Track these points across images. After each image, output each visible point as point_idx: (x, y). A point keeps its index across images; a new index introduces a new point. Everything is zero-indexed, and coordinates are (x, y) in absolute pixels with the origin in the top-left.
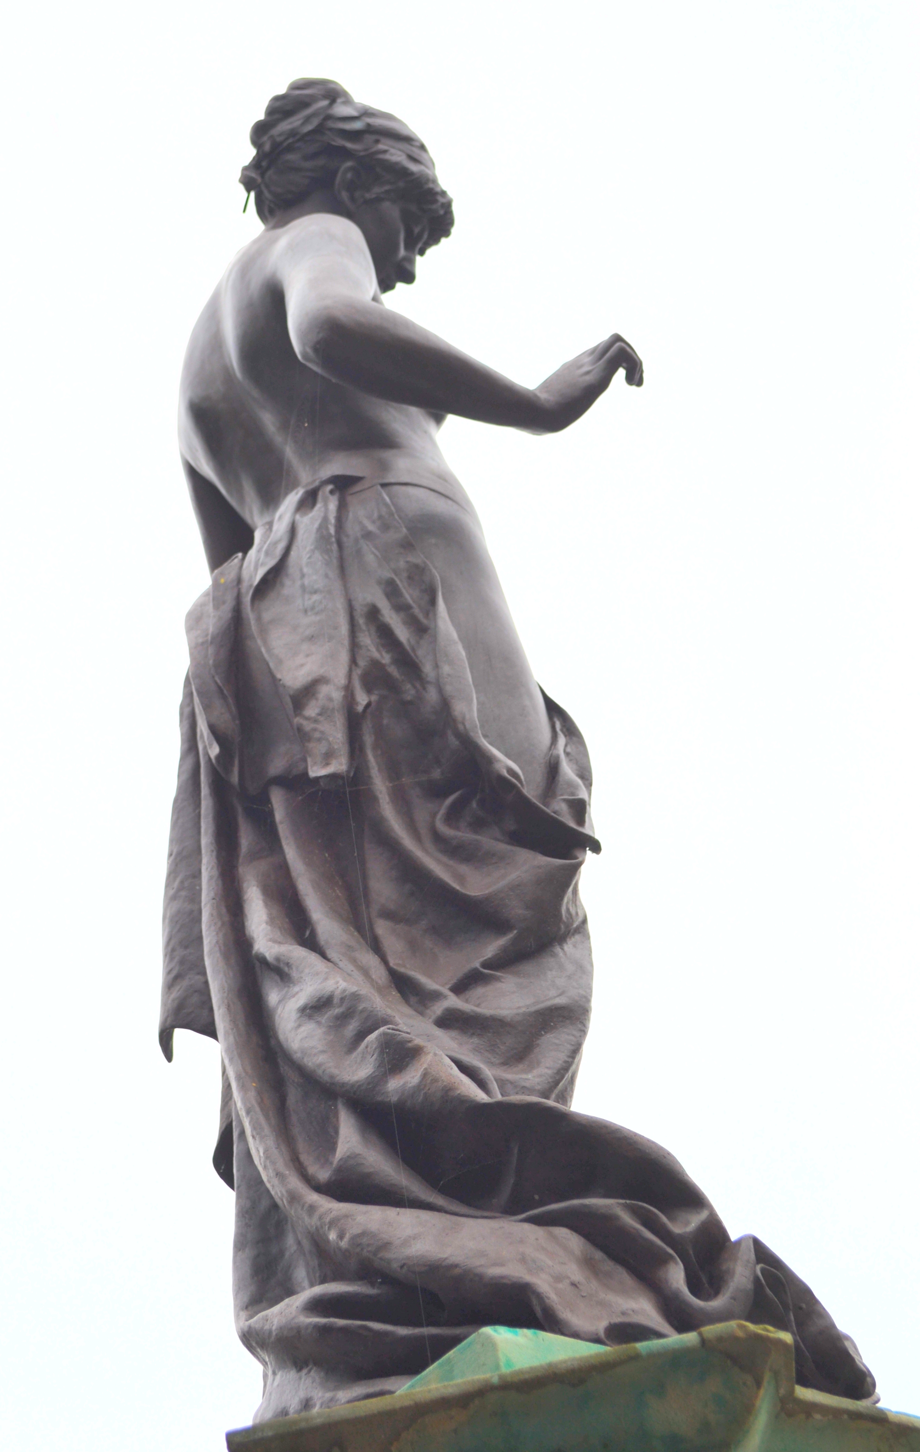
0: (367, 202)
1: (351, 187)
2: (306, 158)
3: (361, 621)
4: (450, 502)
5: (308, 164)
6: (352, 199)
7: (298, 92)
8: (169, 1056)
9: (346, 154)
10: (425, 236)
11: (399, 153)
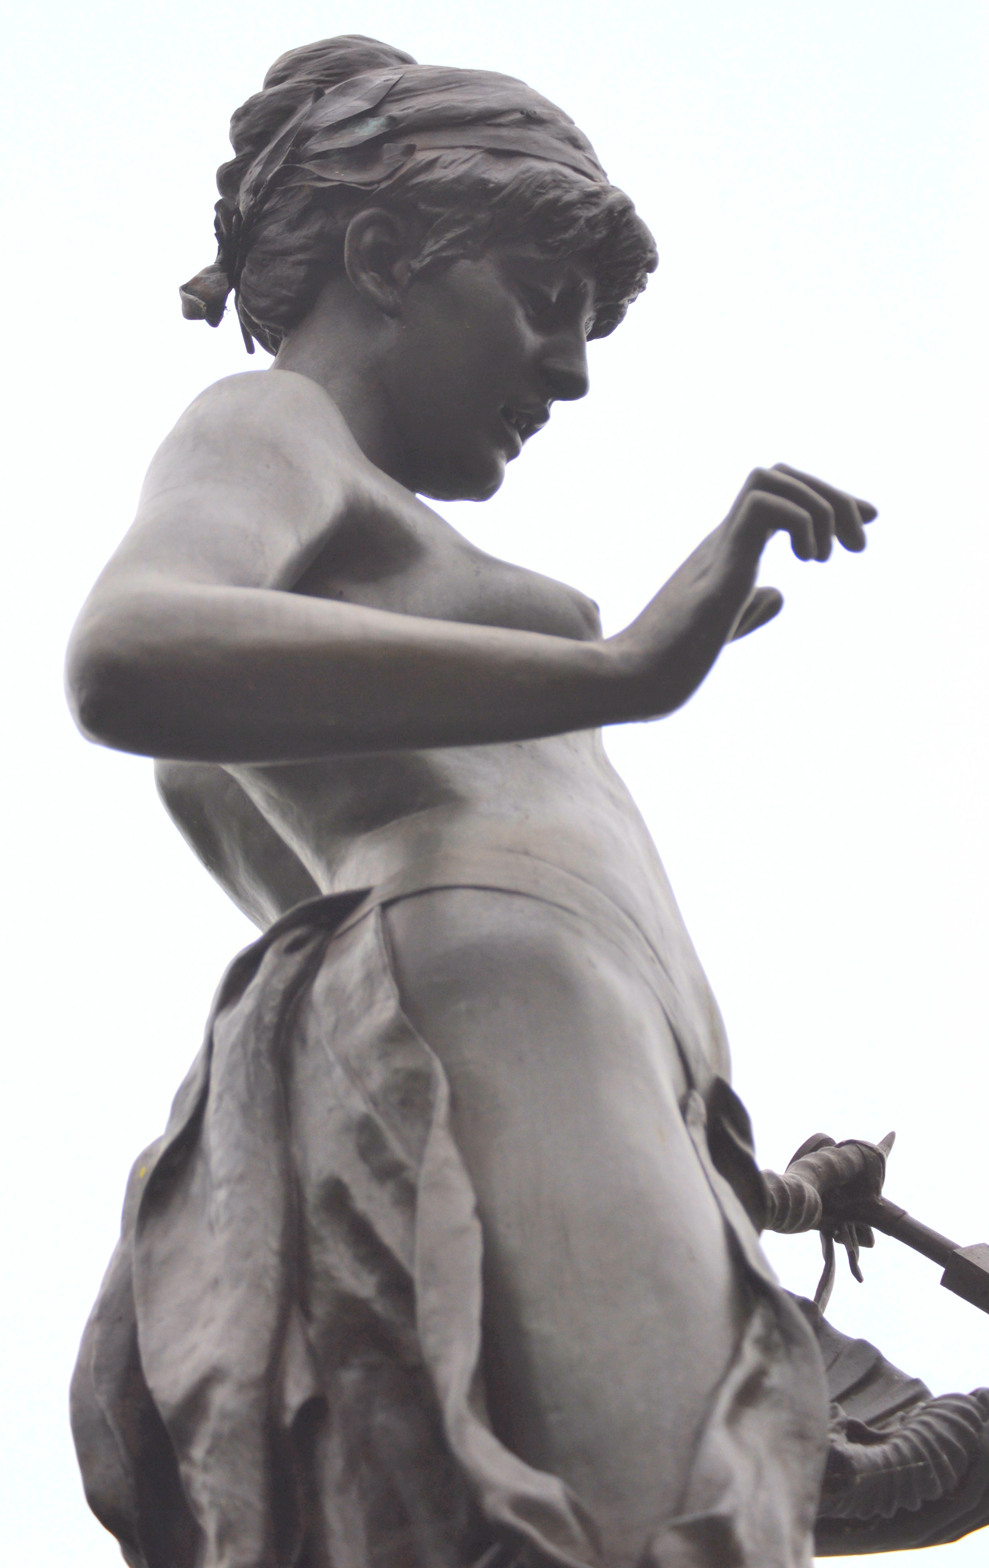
1: (380, 260)
2: (293, 226)
3: (315, 1219)
4: (518, 902)
5: (296, 238)
6: (389, 280)
8: (860, 1279)
9: (348, 197)
10: (590, 285)
11: (464, 154)
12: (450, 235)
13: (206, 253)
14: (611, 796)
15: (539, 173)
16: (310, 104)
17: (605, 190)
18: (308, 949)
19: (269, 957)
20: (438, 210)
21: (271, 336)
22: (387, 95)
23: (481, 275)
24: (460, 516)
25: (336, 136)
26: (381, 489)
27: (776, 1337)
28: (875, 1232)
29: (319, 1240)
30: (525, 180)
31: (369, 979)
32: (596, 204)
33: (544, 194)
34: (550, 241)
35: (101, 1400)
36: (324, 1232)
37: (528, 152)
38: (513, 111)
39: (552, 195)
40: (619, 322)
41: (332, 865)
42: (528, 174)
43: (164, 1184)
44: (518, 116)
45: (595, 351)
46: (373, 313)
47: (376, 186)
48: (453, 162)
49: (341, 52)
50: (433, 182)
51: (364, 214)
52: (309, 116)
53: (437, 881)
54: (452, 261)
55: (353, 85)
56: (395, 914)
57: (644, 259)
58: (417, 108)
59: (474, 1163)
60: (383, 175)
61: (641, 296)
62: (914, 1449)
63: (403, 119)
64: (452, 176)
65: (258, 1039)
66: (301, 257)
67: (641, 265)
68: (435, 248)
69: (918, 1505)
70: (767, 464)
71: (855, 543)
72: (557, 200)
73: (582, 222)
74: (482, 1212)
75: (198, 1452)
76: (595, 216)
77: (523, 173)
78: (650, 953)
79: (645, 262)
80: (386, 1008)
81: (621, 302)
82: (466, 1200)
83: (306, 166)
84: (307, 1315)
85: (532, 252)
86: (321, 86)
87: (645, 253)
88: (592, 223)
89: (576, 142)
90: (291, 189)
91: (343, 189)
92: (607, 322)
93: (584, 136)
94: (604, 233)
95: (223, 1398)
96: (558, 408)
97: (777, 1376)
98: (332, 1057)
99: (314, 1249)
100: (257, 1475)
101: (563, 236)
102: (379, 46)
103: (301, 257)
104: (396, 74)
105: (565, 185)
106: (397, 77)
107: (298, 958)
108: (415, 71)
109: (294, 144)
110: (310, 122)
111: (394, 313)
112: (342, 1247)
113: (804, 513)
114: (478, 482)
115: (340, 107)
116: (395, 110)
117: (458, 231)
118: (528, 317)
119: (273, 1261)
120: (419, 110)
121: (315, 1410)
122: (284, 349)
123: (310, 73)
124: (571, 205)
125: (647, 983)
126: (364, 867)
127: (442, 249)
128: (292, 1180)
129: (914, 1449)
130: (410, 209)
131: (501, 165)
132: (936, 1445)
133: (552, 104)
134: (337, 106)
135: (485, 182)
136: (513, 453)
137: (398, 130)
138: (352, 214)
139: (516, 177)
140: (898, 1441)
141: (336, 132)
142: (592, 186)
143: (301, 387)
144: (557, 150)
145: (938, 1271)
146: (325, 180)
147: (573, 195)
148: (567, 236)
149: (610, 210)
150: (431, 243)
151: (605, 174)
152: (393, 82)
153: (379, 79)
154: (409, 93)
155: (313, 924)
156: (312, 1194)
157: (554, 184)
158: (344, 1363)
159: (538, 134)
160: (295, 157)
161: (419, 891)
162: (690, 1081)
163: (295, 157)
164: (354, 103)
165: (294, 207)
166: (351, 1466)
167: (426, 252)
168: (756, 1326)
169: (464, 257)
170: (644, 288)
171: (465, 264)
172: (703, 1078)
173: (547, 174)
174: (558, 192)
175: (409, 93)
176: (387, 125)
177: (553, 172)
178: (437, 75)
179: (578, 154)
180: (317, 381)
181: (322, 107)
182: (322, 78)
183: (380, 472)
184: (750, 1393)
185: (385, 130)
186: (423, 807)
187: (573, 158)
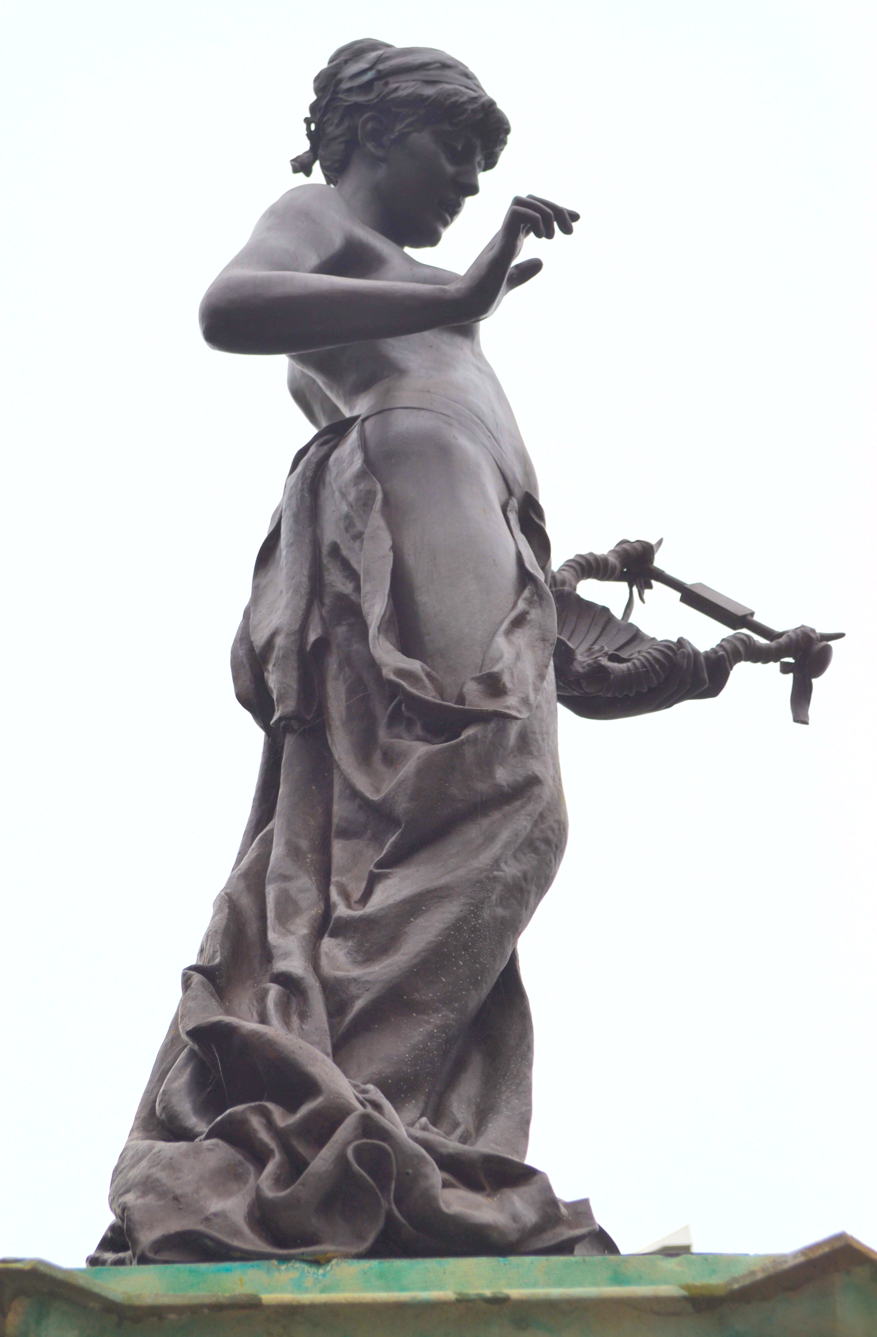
4: (422, 413)
7: (334, 63)
9: (358, 108)
11: (412, 83)
12: (407, 122)
13: (304, 146)
14: (479, 369)
17: (480, 97)
18: (331, 444)
19: (312, 449)
23: (423, 139)
24: (421, 255)
27: (536, 598)
28: (653, 582)
29: (328, 570)
31: (352, 453)
35: (241, 652)
36: (330, 566)
39: (454, 99)
41: (351, 409)
43: (266, 555)
44: (438, 65)
46: (375, 161)
50: (398, 97)
51: (366, 115)
53: (386, 407)
54: (409, 133)
56: (368, 425)
59: (394, 527)
62: (642, 663)
65: (303, 484)
66: (341, 139)
69: (646, 690)
70: (524, 195)
71: (567, 230)
72: (456, 102)
74: (396, 550)
75: (270, 667)
78: (489, 434)
80: (358, 463)
82: (389, 543)
84: (322, 604)
88: (474, 111)
89: (468, 75)
91: (356, 104)
92: (490, 163)
95: (280, 641)
97: (534, 614)
98: (334, 488)
99: (326, 574)
100: (295, 674)
107: (326, 448)
111: (383, 160)
112: (338, 572)
113: (538, 215)
114: (430, 238)
119: (305, 580)
121: (323, 644)
124: (464, 103)
125: (486, 447)
126: (362, 406)
128: (316, 543)
129: (642, 663)
130: (388, 110)
132: (653, 662)
135: (421, 95)
137: (383, 76)
140: (635, 661)
142: (473, 94)
145: (678, 595)
146: (347, 101)
147: (464, 99)
153: (373, 55)
154: (388, 58)
155: (333, 432)
156: (325, 550)
158: (339, 624)
159: (448, 73)
160: (335, 92)
161: (381, 412)
162: (510, 492)
163: (335, 92)
164: (362, 65)
166: (341, 668)
168: (526, 593)
171: (415, 135)
172: (518, 492)
175: (388, 58)
177: (455, 89)
184: (519, 622)
186: (386, 377)
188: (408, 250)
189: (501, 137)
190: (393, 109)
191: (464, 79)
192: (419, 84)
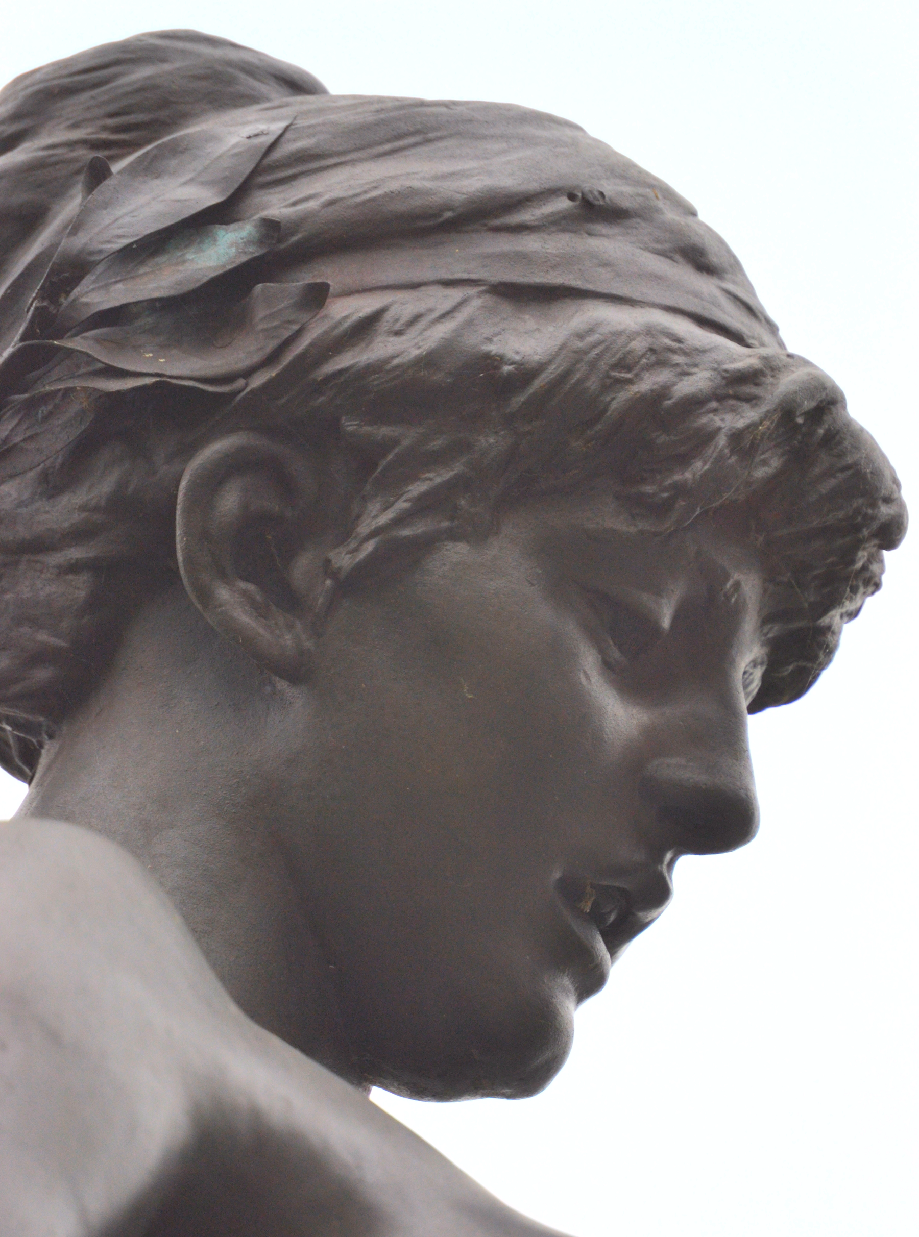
0: (351, 585)
1: (259, 549)
2: (54, 484)
5: (63, 511)
6: (284, 598)
9: (177, 410)
10: (749, 587)
12: (417, 489)
15: (618, 334)
16: (78, 200)
17: (770, 368)
20: (385, 431)
21: (19, 739)
22: (256, 171)
25: (143, 270)
26: (281, 1086)
30: (586, 353)
32: (751, 400)
33: (630, 382)
34: (649, 489)
37: (590, 287)
38: (551, 193)
39: (647, 384)
40: (822, 666)
42: (591, 339)
44: (563, 204)
45: (771, 737)
46: (249, 675)
47: (241, 382)
48: (416, 319)
49: (142, 73)
52: (75, 226)
55: (175, 149)
57: (873, 518)
58: (327, 197)
60: (256, 358)
61: (872, 605)
63: (296, 224)
64: (415, 352)
66: (75, 553)
67: (866, 532)
68: (384, 519)
72: (663, 393)
73: (722, 441)
76: (752, 426)
77: (580, 336)
79: (875, 526)
81: (825, 621)
83: (77, 343)
85: (609, 518)
86: (100, 154)
87: (873, 505)
89: (700, 256)
90: (46, 398)
92: (793, 668)
93: (722, 242)
94: (775, 463)
96: (689, 872)
101: (677, 477)
102: (233, 55)
103: (75, 553)
104: (274, 120)
105: (678, 359)
106: (277, 127)
108: (320, 111)
109: (42, 296)
110: (80, 241)
111: (297, 672)
115: (144, 203)
116: (277, 204)
117: (438, 477)
118: (607, 666)
120: (332, 203)
122: (49, 768)
123: (75, 126)
124: (694, 404)
127: (400, 521)
130: (324, 431)
131: (529, 321)
133: (641, 171)
134: (141, 199)
135: (491, 362)
136: (591, 981)
137: (285, 252)
138: (188, 450)
139: (563, 347)
141: (142, 263)
142: (740, 358)
143: (86, 856)
144: (656, 278)
147: (699, 381)
148: (688, 475)
149: (786, 412)
150: (374, 507)
151: (772, 328)
152: (270, 139)
153: (234, 133)
154: (309, 162)
157: (653, 358)
159: (610, 244)
160: (47, 324)
165: (56, 440)
167: (364, 529)
169: (453, 536)
170: (877, 586)
171: (457, 552)
173: (633, 336)
174: (663, 376)
176: (261, 242)
177: (649, 331)
178: (370, 118)
179: (706, 285)
180: (125, 842)
181: (106, 205)
182: (104, 136)
183: (276, 1042)
185: (255, 251)
187: (697, 295)
188: (379, 1096)
189: (862, 556)
190: (350, 425)
191: (683, 274)
192: (477, 303)
